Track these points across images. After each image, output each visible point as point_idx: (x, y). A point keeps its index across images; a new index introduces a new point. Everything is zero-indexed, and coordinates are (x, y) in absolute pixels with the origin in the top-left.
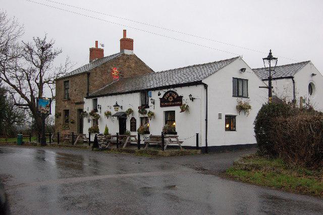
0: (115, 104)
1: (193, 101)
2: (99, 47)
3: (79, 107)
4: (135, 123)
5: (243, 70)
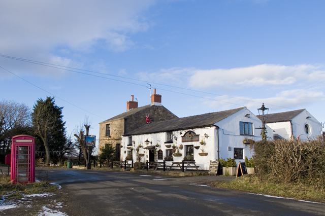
2: (135, 100)
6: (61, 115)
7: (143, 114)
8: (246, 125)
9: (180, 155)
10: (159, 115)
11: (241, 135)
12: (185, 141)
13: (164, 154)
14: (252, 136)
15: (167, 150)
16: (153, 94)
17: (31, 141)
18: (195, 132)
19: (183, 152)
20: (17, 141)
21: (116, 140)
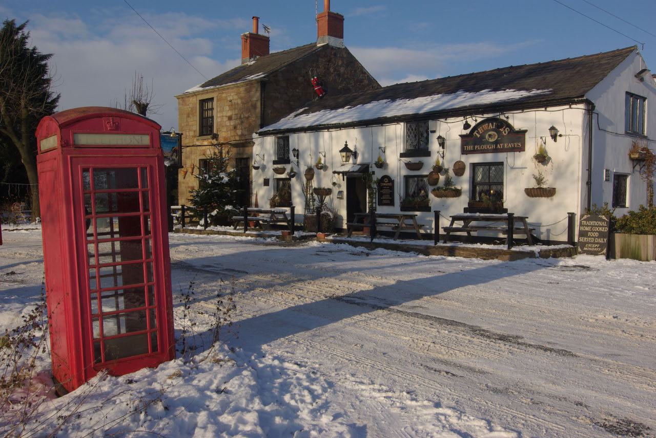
2: (262, 32)
6: (46, 77)
10: (339, 75)
11: (627, 133)
12: (474, 152)
13: (399, 191)
14: (645, 137)
15: (407, 178)
16: (324, 10)
18: (510, 121)
20: (84, 139)
21: (235, 146)
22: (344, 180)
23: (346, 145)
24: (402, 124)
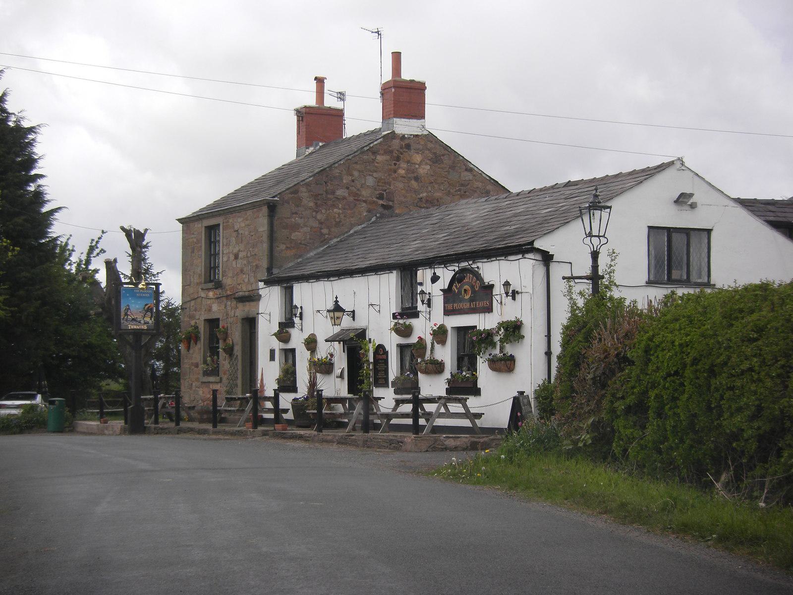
0: (330, 305)
1: (514, 298)
2: (330, 102)
3: (242, 311)
4: (386, 362)
5: (683, 200)
6: (33, 172)
7: (346, 180)
8: (677, 238)
9: (437, 368)
16: (388, 76)
17: (142, 397)
19: (446, 354)
22: (344, 351)
23: (337, 302)
24: (395, 272)
